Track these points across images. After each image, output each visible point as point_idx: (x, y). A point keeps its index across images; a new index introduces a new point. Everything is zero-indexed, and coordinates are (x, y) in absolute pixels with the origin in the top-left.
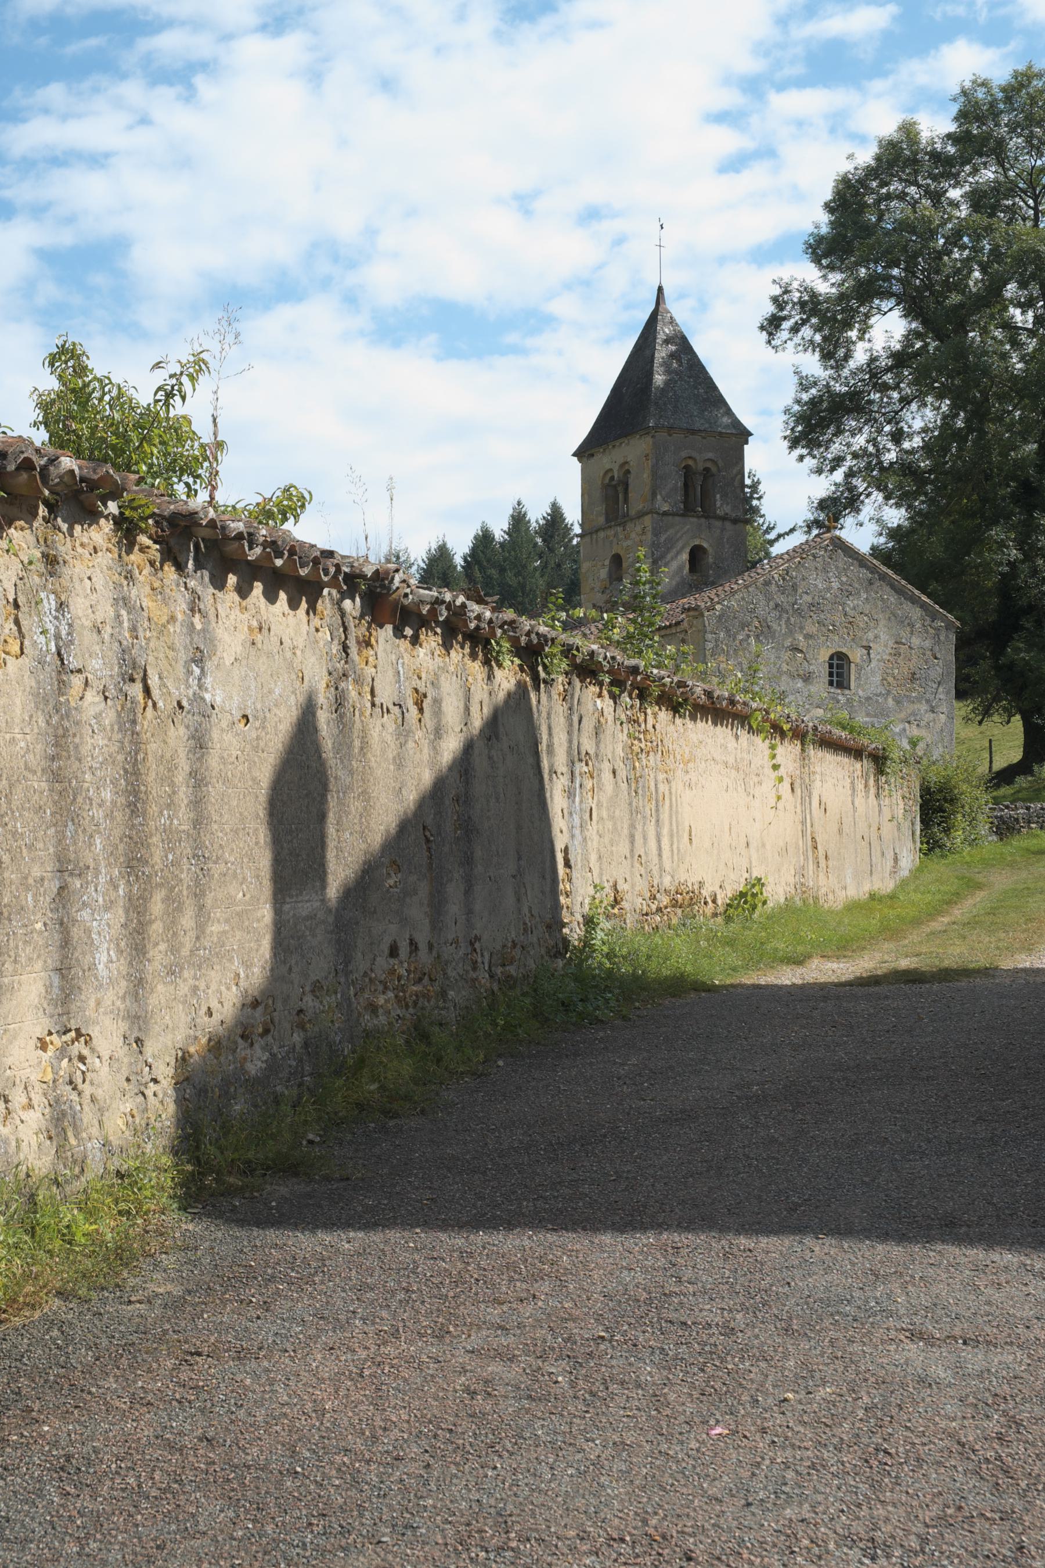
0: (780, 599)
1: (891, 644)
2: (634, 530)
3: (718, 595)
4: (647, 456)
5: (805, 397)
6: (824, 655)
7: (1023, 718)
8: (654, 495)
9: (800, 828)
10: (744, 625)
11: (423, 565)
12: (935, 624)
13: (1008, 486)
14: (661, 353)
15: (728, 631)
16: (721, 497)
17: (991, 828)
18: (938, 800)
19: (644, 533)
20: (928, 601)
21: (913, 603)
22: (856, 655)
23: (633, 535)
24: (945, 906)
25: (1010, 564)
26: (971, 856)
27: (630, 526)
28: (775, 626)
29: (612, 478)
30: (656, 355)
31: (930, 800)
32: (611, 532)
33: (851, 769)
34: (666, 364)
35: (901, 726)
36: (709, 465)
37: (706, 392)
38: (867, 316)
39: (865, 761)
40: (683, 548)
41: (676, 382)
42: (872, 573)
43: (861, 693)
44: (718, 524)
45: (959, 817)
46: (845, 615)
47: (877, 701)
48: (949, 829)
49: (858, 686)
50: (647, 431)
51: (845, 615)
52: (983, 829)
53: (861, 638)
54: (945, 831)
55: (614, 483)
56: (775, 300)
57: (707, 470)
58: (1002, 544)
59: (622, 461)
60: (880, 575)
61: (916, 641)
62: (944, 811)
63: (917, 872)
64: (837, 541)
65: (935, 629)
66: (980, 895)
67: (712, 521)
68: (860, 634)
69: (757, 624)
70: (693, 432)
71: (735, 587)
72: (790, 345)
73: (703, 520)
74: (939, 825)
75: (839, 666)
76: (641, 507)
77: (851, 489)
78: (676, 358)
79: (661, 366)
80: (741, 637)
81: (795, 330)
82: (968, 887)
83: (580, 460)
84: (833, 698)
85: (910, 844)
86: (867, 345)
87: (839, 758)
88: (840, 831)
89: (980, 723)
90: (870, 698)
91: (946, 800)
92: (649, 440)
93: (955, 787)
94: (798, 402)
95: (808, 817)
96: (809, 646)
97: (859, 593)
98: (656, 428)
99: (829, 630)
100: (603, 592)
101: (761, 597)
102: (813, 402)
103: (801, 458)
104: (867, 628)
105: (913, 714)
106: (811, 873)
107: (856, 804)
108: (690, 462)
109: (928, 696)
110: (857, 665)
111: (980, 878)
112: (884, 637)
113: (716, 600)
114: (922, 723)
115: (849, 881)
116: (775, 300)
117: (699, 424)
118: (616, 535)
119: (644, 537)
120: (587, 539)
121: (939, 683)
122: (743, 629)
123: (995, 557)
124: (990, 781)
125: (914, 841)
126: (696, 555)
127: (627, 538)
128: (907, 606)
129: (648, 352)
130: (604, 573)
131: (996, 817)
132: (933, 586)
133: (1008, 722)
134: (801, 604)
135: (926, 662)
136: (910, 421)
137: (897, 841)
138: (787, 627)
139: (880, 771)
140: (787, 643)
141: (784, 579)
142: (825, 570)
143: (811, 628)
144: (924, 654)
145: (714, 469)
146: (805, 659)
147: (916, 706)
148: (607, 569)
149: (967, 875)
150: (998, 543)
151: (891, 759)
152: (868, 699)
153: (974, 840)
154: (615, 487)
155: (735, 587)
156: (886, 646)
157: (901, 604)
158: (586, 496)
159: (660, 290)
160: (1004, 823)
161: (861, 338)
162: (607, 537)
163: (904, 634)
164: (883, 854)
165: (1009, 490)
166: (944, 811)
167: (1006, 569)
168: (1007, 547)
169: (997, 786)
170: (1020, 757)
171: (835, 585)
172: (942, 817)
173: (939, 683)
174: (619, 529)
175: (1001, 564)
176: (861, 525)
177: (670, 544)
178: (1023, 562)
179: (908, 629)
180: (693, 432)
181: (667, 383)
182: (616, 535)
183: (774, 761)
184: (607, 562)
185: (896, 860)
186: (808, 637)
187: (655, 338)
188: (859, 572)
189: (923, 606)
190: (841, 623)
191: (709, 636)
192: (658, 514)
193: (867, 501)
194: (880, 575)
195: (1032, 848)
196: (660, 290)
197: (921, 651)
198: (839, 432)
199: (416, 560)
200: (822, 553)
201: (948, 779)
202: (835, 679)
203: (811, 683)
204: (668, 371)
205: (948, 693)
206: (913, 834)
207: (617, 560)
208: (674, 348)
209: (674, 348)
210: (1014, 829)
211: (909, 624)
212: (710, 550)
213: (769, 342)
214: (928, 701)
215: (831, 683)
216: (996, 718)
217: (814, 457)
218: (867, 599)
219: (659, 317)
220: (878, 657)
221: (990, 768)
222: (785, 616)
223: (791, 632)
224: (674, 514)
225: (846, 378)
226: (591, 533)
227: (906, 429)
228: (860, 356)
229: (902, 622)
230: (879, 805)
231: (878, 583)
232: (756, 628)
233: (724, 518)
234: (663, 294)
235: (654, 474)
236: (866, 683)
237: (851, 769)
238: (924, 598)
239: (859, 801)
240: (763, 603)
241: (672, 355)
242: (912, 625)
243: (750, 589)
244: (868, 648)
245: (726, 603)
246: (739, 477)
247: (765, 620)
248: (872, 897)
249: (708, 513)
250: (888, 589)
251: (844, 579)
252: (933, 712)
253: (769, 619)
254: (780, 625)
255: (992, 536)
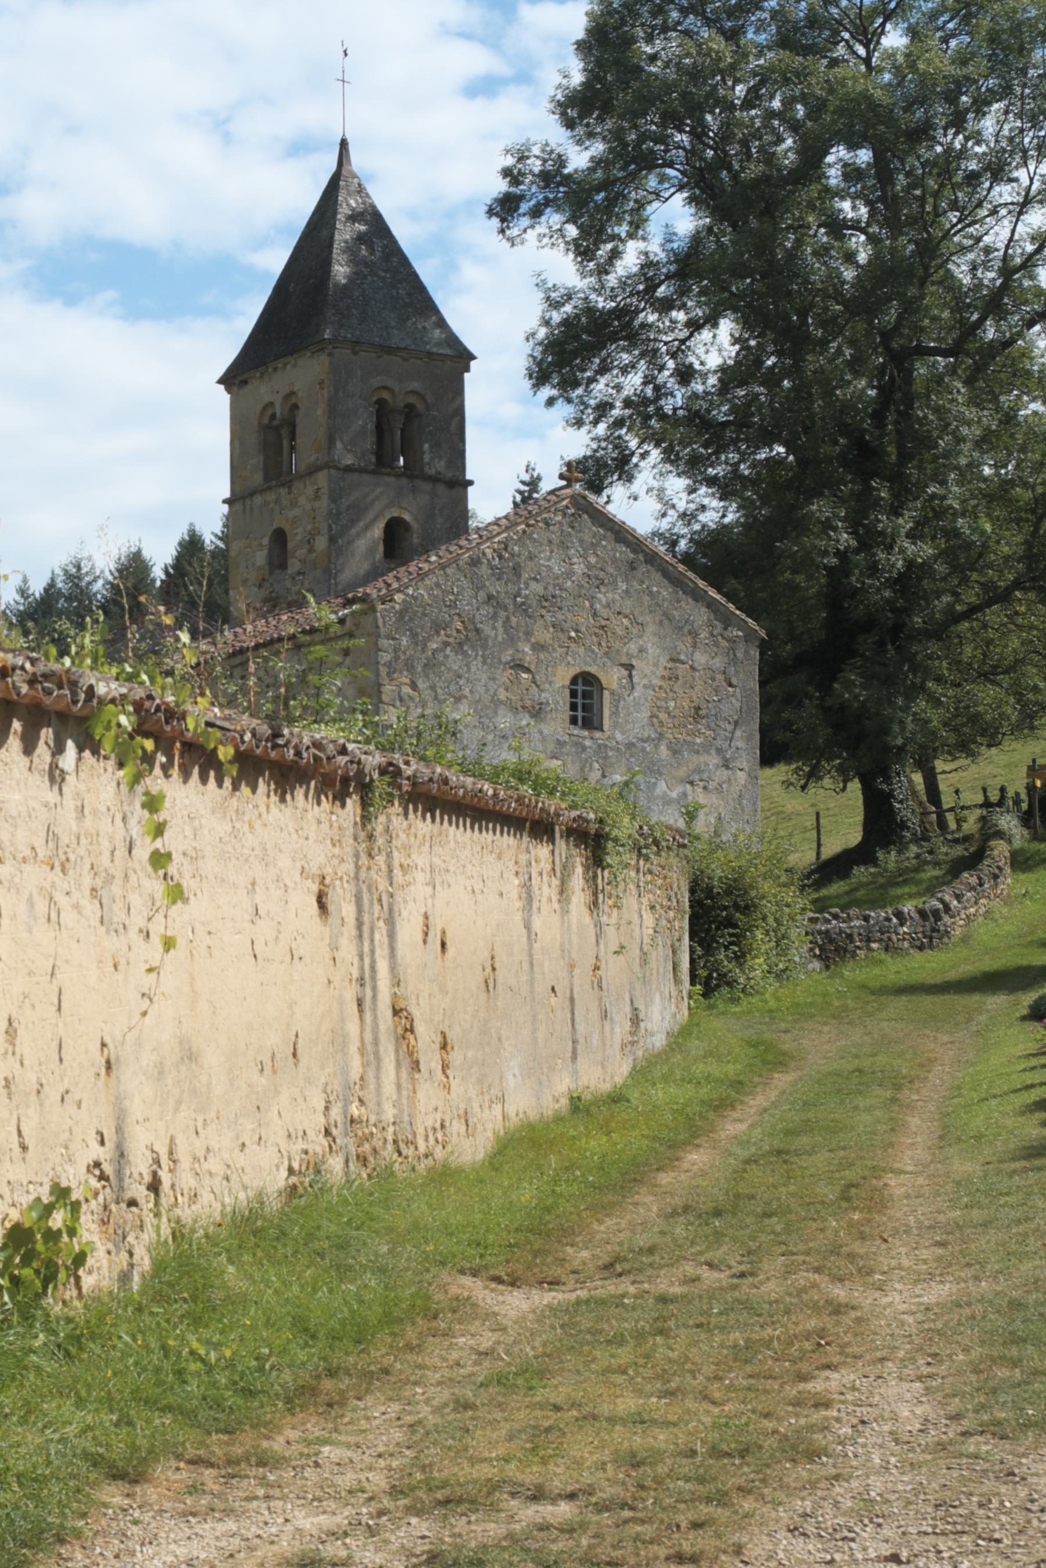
0: (496, 587)
1: (663, 661)
2: (304, 491)
3: (398, 579)
4: (321, 383)
5: (556, 317)
6: (563, 676)
7: (862, 782)
8: (331, 440)
9: (350, 994)
10: (438, 627)
11: (110, 578)
12: (727, 634)
13: (836, 443)
14: (344, 233)
15: (414, 635)
16: (431, 447)
17: (811, 950)
18: (725, 908)
19: (317, 497)
20: (718, 597)
21: (696, 600)
22: (612, 678)
23: (302, 501)
24: (711, 1115)
25: (838, 553)
26: (778, 999)
27: (297, 486)
28: (487, 629)
29: (273, 416)
30: (337, 237)
31: (712, 908)
32: (271, 496)
33: (523, 858)
34: (350, 250)
35: (680, 789)
36: (412, 399)
37: (409, 295)
38: (641, 205)
39: (561, 844)
40: (375, 519)
41: (365, 277)
42: (634, 551)
43: (619, 736)
44: (427, 487)
45: (759, 935)
46: (595, 615)
47: (643, 750)
48: (743, 955)
49: (615, 725)
50: (321, 346)
51: (595, 615)
52: (799, 949)
53: (618, 652)
54: (737, 958)
55: (276, 423)
56: (507, 172)
57: (410, 407)
58: (827, 526)
59: (286, 390)
60: (646, 555)
61: (701, 658)
62: (735, 926)
63: (679, 1038)
64: (582, 501)
65: (729, 640)
66: (782, 1080)
67: (418, 483)
68: (616, 645)
69: (459, 625)
70: (390, 350)
71: (426, 567)
72: (531, 235)
73: (404, 481)
74: (726, 948)
75: (586, 695)
76: (312, 459)
77: (619, 445)
78: (365, 243)
79: (344, 252)
80: (435, 646)
81: (536, 213)
82: (764, 1062)
83: (228, 390)
84: (577, 744)
85: (669, 987)
86: (641, 245)
87: (488, 837)
88: (488, 986)
89: (803, 788)
90: (633, 745)
91: (737, 907)
92: (324, 359)
93: (751, 887)
94: (547, 323)
95: (383, 967)
96: (539, 662)
97: (614, 583)
98: (334, 341)
99: (570, 638)
100: (260, 586)
101: (465, 583)
102: (567, 323)
103: (550, 402)
104: (627, 637)
105: (698, 770)
106: (389, 1089)
107: (537, 924)
108: (385, 395)
109: (719, 742)
110: (612, 693)
111: (787, 1044)
112: (652, 650)
113: (395, 585)
114: (712, 785)
115: (511, 1082)
116: (507, 172)
117: (397, 339)
118: (277, 501)
119: (317, 504)
120: (238, 506)
121: (736, 723)
122: (438, 633)
123: (817, 542)
124: (808, 876)
125: (677, 981)
126: (394, 531)
127: (294, 504)
128: (688, 605)
129: (325, 233)
130: (261, 558)
131: (820, 932)
132: (733, 583)
133: (844, 789)
134: (526, 597)
135: (717, 691)
136: (703, 357)
137: (638, 986)
138: (506, 632)
139: (597, 861)
140: (507, 656)
141: (500, 557)
142: (563, 545)
143: (543, 634)
144: (713, 679)
145: (420, 407)
146: (534, 682)
147: (702, 759)
148: (265, 552)
149: (767, 1036)
150: (821, 522)
151: (616, 840)
152: (630, 745)
153: (784, 971)
154: (277, 429)
155: (426, 567)
156: (656, 665)
157: (678, 601)
158: (237, 443)
159: (344, 144)
160: (831, 941)
161: (631, 236)
162: (266, 503)
163: (683, 647)
164: (605, 1015)
165: (837, 448)
166: (735, 926)
167: (834, 561)
168: (835, 529)
169: (818, 885)
170: (860, 839)
171: (579, 568)
172: (731, 935)
173: (736, 723)
174: (283, 491)
175: (825, 553)
176: (636, 499)
177: (357, 511)
178: (857, 551)
179: (689, 639)
180: (390, 350)
181: (352, 279)
182: (277, 501)
183: (158, 844)
184: (266, 541)
185: (636, 1020)
186: (538, 647)
187: (335, 213)
188: (614, 550)
189: (711, 604)
190: (588, 628)
191: (384, 643)
192: (338, 469)
193: (642, 464)
194: (646, 555)
195: (871, 984)
196: (344, 144)
197: (709, 674)
198: (603, 370)
199: (102, 572)
200: (559, 518)
201: (742, 872)
202: (580, 714)
203: (543, 720)
204: (354, 260)
205: (749, 739)
206: (675, 968)
207: (280, 537)
208: (363, 228)
209: (363, 228)
210: (846, 950)
211: (690, 633)
212: (414, 525)
213: (502, 231)
214: (719, 751)
215: (574, 721)
216: (827, 782)
217: (569, 401)
218: (627, 591)
219: (342, 183)
220: (645, 681)
221: (818, 854)
222: (503, 614)
223: (511, 640)
224: (361, 471)
225: (612, 289)
226: (243, 498)
227: (697, 366)
228: (630, 260)
229: (681, 629)
230: (599, 925)
231: (643, 568)
232: (458, 631)
233: (435, 479)
234: (347, 150)
235: (332, 411)
236: (627, 721)
237: (523, 858)
238: (713, 593)
239: (545, 921)
240: (468, 592)
241: (361, 238)
242: (694, 634)
243: (449, 571)
244: (630, 667)
245: (410, 591)
246: (457, 419)
247: (472, 620)
248: (577, 1105)
249: (412, 472)
250: (657, 576)
251: (593, 560)
252: (727, 767)
253: (478, 618)
254: (494, 628)
255: (813, 513)
